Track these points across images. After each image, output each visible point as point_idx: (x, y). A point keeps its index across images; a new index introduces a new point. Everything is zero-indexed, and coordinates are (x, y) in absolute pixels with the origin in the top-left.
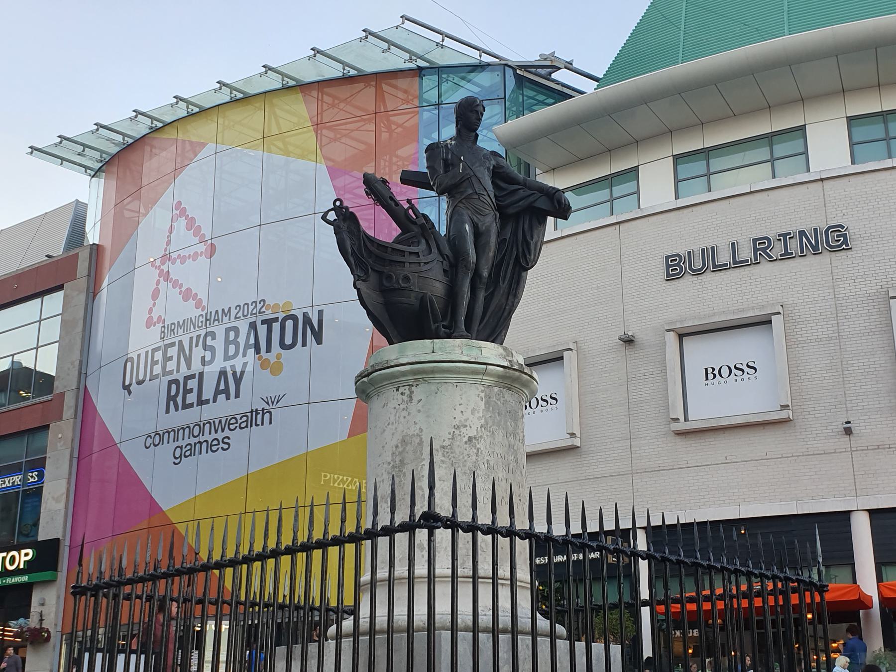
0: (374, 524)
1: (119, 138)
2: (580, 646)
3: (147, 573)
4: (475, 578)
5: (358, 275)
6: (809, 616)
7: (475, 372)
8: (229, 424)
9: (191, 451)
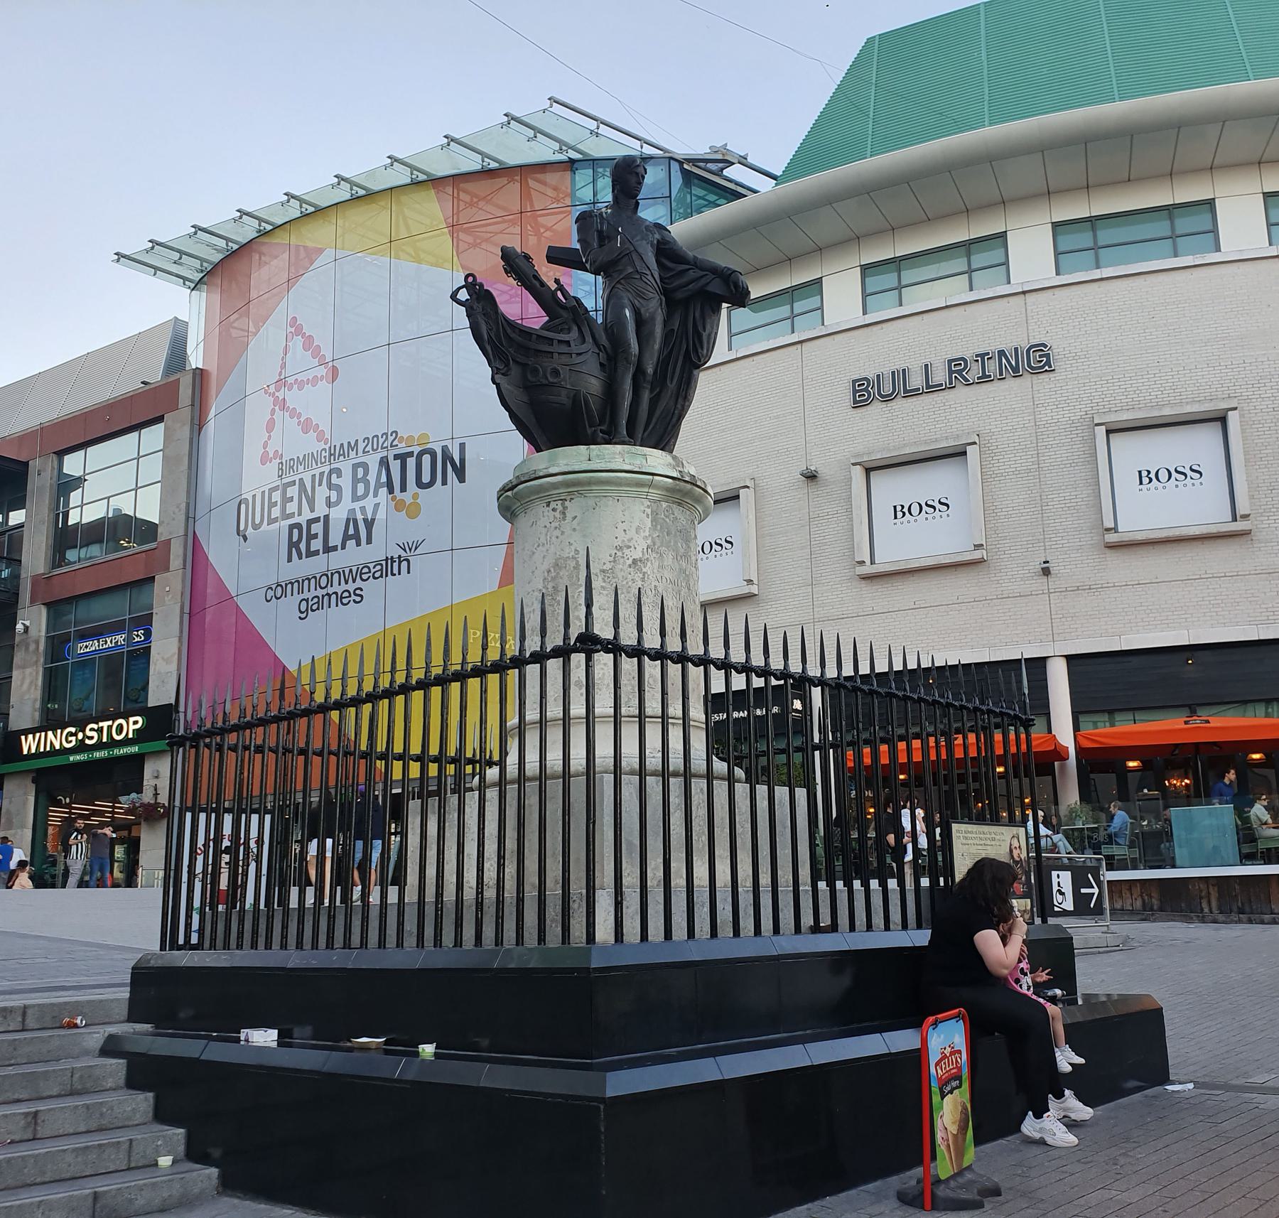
0: (522, 649)
1: (222, 243)
2: (762, 790)
3: (255, 717)
4: (642, 717)
5: (497, 368)
6: (1000, 769)
7: (640, 484)
8: (361, 574)
9: (318, 604)
